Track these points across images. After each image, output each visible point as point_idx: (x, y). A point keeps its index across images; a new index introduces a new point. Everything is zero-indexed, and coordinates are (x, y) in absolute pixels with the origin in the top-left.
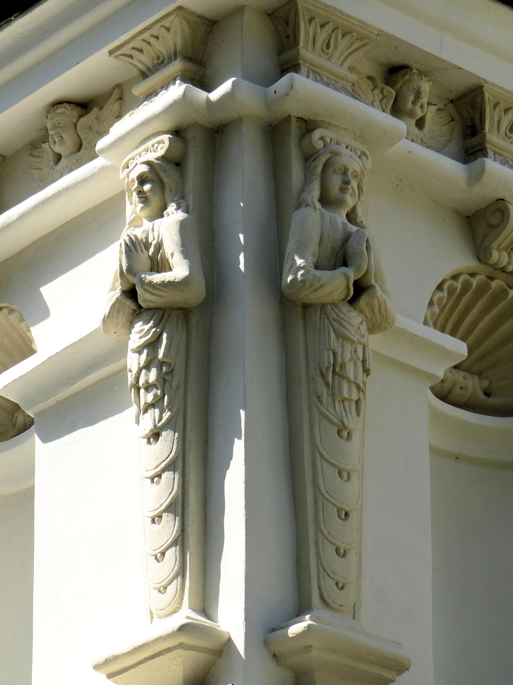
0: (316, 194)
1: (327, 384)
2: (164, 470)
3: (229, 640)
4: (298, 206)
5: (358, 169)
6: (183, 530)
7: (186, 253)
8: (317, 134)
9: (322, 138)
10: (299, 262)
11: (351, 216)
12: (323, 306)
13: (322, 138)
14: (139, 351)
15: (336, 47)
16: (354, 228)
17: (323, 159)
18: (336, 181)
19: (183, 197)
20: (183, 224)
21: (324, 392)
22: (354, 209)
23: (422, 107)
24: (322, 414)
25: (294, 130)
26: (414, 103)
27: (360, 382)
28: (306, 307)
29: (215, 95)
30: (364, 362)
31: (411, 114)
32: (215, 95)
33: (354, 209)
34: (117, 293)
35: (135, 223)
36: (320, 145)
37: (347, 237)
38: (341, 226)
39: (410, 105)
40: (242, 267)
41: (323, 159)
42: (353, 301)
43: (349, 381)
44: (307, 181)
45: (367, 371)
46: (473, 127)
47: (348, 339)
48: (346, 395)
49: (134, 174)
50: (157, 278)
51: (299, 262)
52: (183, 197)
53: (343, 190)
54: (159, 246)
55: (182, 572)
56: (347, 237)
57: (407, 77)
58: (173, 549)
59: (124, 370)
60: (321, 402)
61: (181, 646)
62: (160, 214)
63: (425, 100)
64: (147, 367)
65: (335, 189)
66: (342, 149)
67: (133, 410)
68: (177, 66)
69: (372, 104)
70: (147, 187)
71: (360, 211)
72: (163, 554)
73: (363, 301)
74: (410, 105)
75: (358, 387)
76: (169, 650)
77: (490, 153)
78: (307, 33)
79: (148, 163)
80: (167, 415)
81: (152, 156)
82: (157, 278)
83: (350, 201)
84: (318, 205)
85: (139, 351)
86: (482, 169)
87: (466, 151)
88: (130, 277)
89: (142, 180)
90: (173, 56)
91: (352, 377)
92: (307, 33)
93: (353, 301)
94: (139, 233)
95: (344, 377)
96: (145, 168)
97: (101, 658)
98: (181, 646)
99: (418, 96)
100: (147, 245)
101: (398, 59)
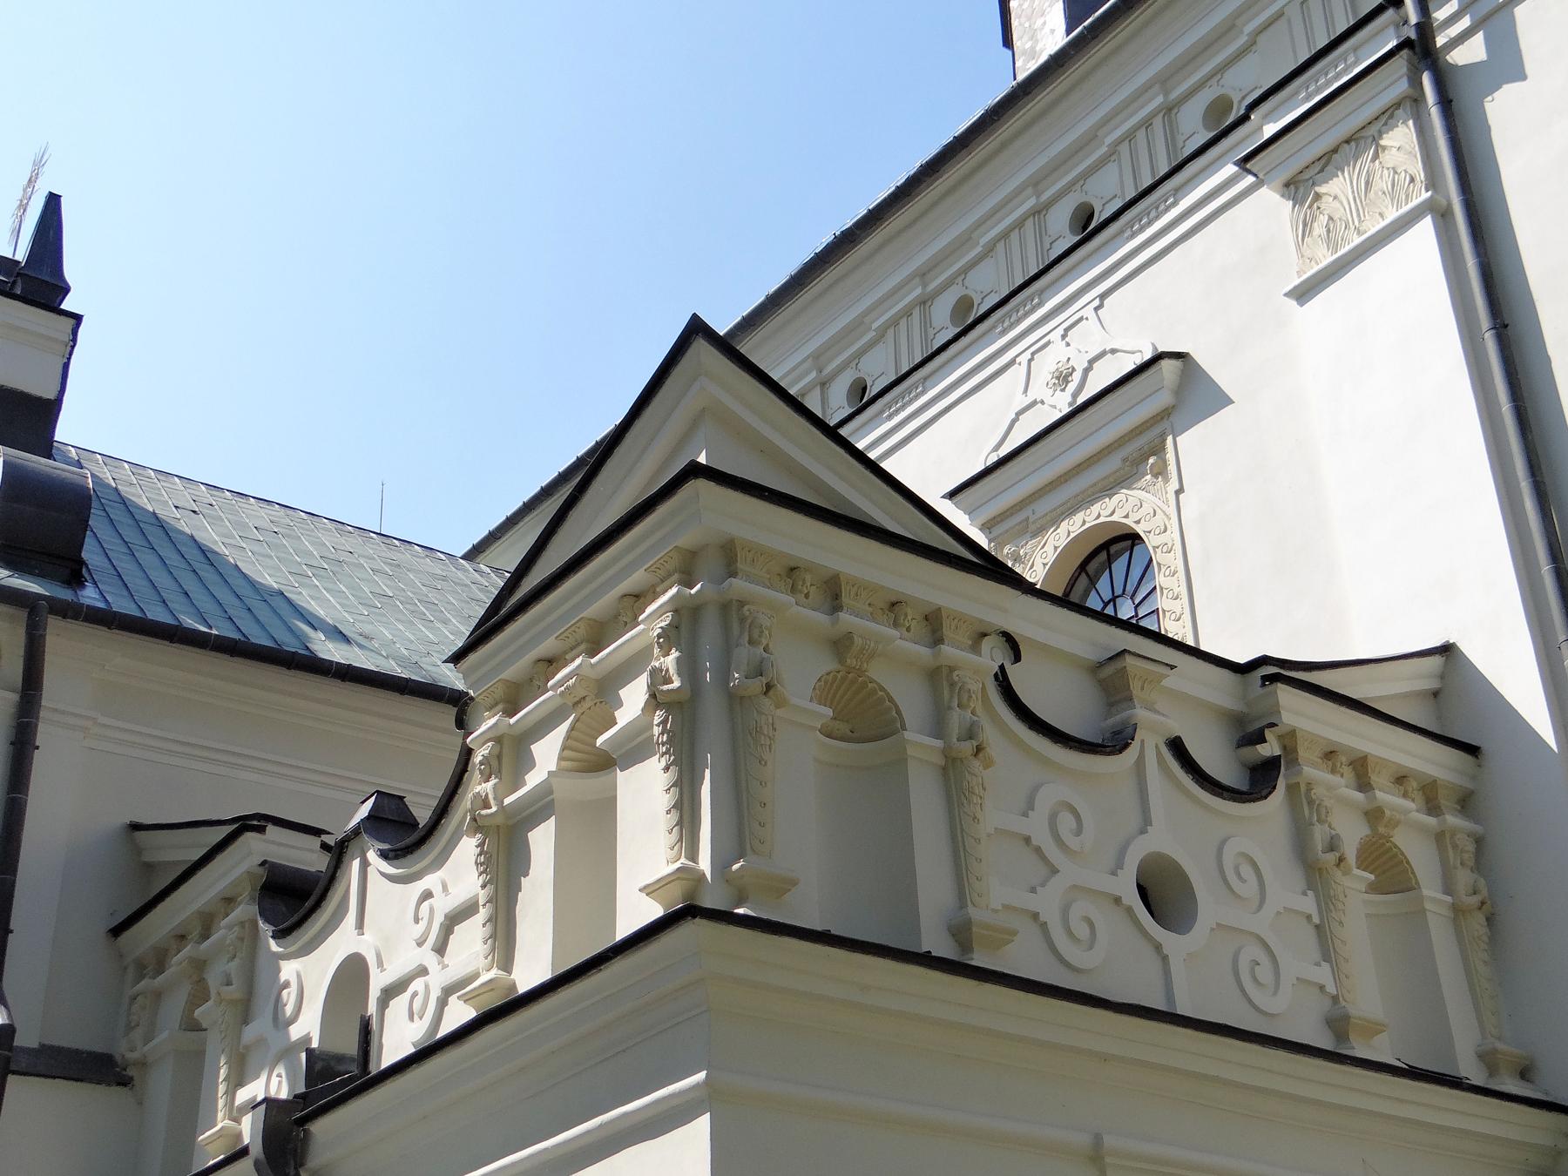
0: (747, 639)
1: (753, 738)
2: (671, 787)
3: (704, 874)
4: (737, 645)
5: (769, 625)
6: (681, 817)
7: (679, 675)
8: (746, 608)
9: (749, 610)
10: (736, 675)
11: (1330, 826)
12: (750, 697)
13: (749, 610)
14: (658, 725)
15: (758, 561)
16: (976, 718)
17: (749, 621)
18: (965, 696)
19: (680, 645)
20: (678, 659)
21: (1332, 907)
22: (768, 645)
23: (807, 587)
24: (964, 812)
25: (1448, 836)
26: (904, 620)
27: (771, 735)
28: (742, 698)
29: (693, 591)
30: (773, 724)
31: (801, 592)
32: (693, 591)
33: (768, 645)
34: (647, 696)
35: (658, 659)
36: (956, 679)
37: (973, 724)
38: (968, 720)
39: (800, 587)
40: (708, 679)
41: (749, 621)
42: (976, 755)
43: (764, 735)
44: (741, 633)
45: (984, 789)
46: (837, 595)
47: (764, 714)
48: (763, 742)
49: (655, 634)
50: (665, 687)
51: (736, 675)
52: (680, 645)
53: (969, 701)
54: (667, 670)
55: (680, 840)
56: (973, 724)
57: (798, 573)
58: (676, 828)
59: (653, 736)
60: (750, 747)
61: (678, 879)
62: (667, 654)
63: (910, 618)
64: (663, 733)
65: (965, 701)
66: (967, 680)
67: (658, 756)
68: (676, 577)
69: (1323, 771)
70: (661, 640)
71: (770, 646)
72: (672, 830)
73: (771, 693)
74: (800, 587)
75: (981, 798)
76: (673, 881)
77: (946, 642)
78: (845, 589)
79: (661, 628)
80: (672, 758)
81: (663, 624)
82: (665, 687)
83: (764, 642)
84: (747, 645)
85: (658, 725)
86: (838, 619)
87: (833, 608)
88: (653, 688)
89: (659, 636)
90: (675, 571)
91: (766, 733)
92: (845, 589)
93: (976, 755)
94: (657, 664)
95: (973, 793)
96: (659, 631)
97: (642, 884)
98: (678, 879)
99: (906, 615)
100: (661, 670)
101: (793, 564)
